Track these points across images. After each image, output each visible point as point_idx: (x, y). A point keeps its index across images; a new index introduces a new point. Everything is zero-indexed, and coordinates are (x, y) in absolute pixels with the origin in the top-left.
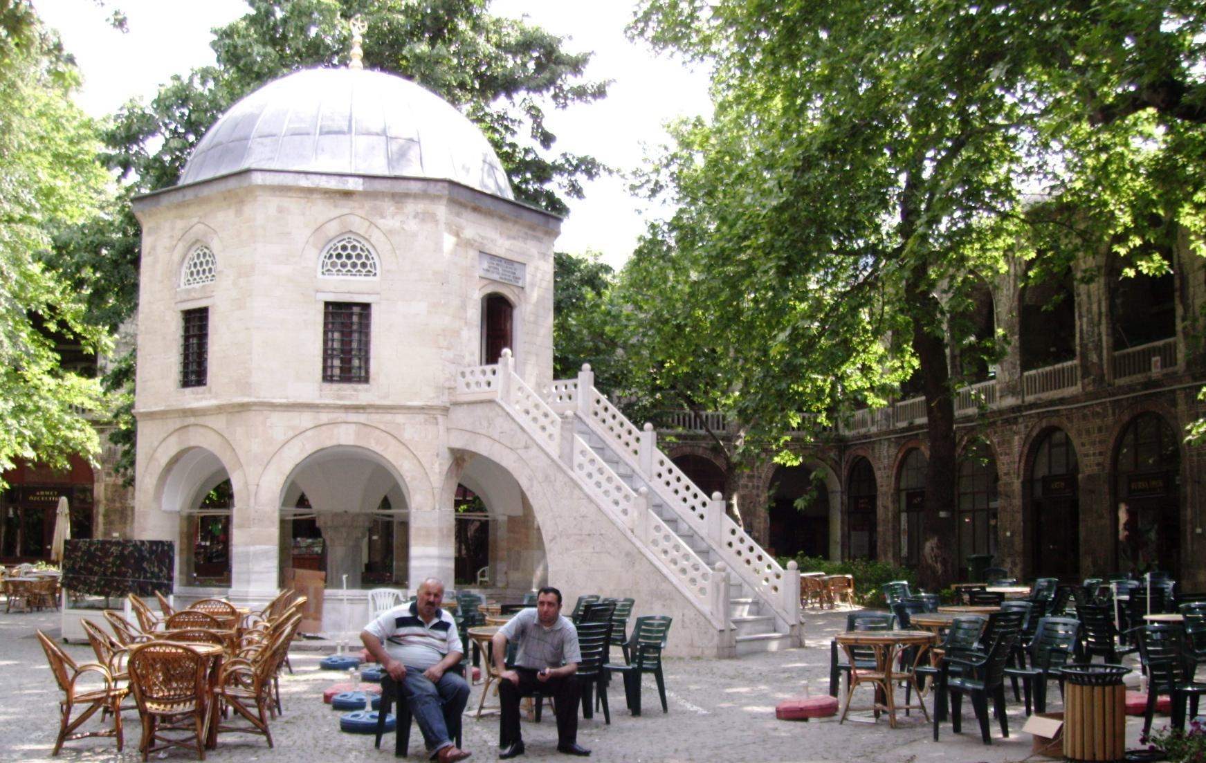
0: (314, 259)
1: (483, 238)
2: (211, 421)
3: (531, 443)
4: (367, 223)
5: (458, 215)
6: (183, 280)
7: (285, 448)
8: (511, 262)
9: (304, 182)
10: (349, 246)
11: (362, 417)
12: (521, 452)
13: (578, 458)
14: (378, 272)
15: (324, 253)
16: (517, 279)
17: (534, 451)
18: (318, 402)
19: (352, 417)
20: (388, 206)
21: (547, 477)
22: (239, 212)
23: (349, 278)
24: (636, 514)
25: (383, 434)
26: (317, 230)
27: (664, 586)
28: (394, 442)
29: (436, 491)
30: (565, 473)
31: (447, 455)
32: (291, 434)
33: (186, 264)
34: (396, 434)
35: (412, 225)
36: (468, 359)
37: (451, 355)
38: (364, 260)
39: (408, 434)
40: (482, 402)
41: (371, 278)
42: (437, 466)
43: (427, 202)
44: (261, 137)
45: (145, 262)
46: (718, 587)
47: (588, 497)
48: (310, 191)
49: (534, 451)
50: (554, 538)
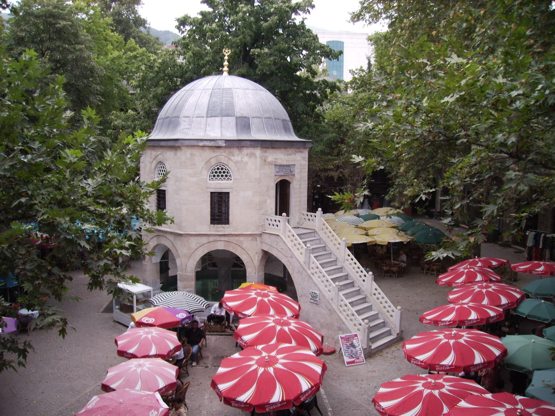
0: (206, 174)
1: (276, 159)
2: (169, 236)
3: (292, 256)
5: (265, 152)
6: (156, 176)
8: (289, 166)
9: (201, 144)
11: (226, 239)
12: (290, 259)
13: (312, 265)
15: (210, 171)
16: (291, 172)
18: (209, 233)
19: (223, 238)
20: (236, 151)
22: (175, 155)
23: (220, 181)
24: (334, 293)
27: (343, 326)
31: (261, 252)
32: (198, 245)
35: (246, 159)
36: (270, 211)
37: (262, 212)
38: (226, 174)
40: (274, 234)
41: (229, 181)
42: (256, 257)
46: (365, 331)
47: (315, 283)
48: (204, 147)
49: (294, 259)
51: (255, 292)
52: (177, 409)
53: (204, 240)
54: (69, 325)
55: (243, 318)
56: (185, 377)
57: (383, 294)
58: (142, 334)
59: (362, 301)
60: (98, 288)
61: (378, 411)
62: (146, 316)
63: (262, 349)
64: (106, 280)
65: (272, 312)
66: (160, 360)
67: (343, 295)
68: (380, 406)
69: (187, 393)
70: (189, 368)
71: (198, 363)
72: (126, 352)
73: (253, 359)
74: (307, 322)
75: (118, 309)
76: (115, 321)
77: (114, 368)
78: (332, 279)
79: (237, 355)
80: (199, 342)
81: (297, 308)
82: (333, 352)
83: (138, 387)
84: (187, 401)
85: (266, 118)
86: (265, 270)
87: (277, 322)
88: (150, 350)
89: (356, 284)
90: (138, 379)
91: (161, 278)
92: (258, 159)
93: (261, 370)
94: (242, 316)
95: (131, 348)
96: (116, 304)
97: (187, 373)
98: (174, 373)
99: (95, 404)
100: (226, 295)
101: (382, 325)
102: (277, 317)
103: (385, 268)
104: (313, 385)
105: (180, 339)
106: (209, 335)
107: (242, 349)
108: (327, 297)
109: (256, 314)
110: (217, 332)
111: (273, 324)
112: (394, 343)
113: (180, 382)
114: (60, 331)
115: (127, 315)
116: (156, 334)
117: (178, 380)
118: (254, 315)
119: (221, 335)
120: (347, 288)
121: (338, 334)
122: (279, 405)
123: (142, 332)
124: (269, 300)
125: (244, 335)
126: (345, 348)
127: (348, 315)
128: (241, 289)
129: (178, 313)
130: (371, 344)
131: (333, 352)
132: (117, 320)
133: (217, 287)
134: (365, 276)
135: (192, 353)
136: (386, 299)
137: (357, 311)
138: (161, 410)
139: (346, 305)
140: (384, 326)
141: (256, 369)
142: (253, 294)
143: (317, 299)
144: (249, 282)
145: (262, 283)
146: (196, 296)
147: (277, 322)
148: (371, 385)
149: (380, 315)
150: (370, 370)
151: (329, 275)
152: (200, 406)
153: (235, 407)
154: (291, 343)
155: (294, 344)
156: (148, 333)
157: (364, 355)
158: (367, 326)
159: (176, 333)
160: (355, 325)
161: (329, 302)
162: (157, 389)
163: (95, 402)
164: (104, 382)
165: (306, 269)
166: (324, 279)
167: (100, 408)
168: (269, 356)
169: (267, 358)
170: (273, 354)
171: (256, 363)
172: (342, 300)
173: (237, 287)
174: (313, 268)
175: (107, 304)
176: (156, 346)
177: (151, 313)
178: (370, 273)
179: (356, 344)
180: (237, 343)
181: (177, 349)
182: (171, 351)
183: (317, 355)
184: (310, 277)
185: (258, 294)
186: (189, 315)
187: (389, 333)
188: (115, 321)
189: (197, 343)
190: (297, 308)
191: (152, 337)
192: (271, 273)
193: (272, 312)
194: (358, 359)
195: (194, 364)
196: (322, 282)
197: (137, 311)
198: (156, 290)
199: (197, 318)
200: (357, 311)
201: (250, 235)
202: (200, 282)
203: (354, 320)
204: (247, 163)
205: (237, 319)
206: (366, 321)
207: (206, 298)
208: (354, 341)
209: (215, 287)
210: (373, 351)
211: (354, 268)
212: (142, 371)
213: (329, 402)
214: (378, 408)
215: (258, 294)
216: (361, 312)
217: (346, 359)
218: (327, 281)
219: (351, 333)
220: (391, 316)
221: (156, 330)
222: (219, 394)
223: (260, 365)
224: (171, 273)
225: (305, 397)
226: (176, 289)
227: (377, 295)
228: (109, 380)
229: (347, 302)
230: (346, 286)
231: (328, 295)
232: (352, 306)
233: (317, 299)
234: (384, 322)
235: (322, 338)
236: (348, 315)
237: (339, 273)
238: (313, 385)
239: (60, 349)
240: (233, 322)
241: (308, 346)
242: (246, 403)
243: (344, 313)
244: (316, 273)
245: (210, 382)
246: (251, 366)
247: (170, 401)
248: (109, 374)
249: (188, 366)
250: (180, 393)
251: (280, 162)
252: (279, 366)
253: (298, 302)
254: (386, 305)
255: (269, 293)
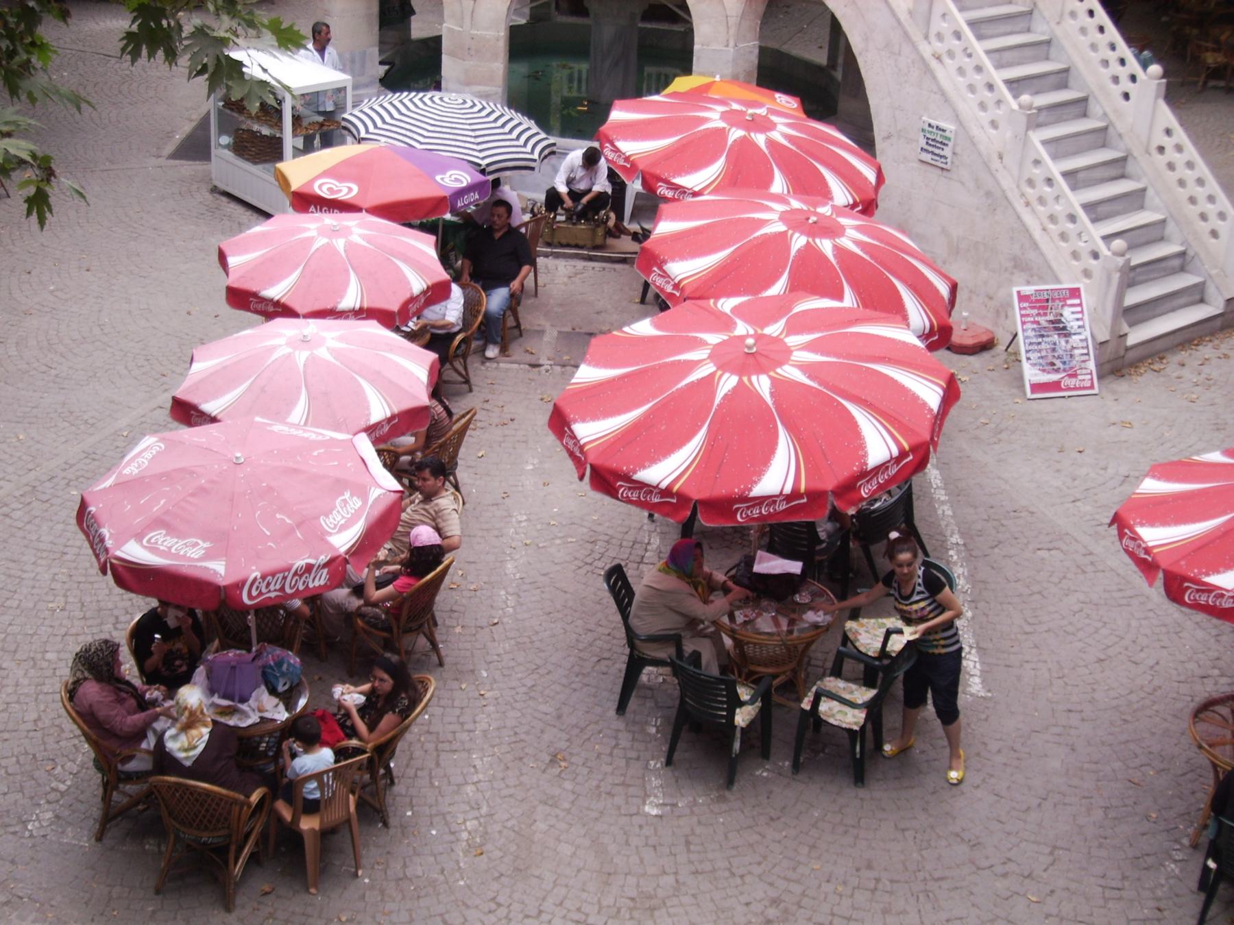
13: (938, 25)
24: (1009, 134)
27: (1031, 255)
29: (732, 21)
30: (915, 47)
45: (375, 454)
47: (943, 93)
51: (721, 109)
52: (428, 497)
54: (64, 182)
55: (673, 200)
56: (459, 394)
57: (1191, 152)
58: (313, 233)
59: (1112, 172)
60: (160, 54)
61: (1131, 554)
62: (326, 174)
63: (735, 310)
64: (187, 29)
65: (779, 184)
66: (373, 328)
67: (1045, 143)
68: (1136, 538)
69: (462, 451)
70: (474, 364)
71: (504, 350)
72: (255, 295)
73: (702, 343)
74: (903, 232)
75: (227, 147)
76: (215, 190)
77: (214, 346)
78: (1009, 83)
79: (644, 327)
80: (514, 278)
81: (871, 176)
82: (986, 346)
83: (299, 412)
84: (462, 474)
86: (761, 37)
87: (796, 221)
88: (342, 292)
89: (1094, 108)
90: (299, 388)
91: (382, 43)
93: (728, 383)
94: (669, 194)
95: (272, 282)
96: (222, 131)
97: (467, 381)
98: (422, 375)
99: (151, 461)
100: (618, 115)
101: (1176, 263)
102: (796, 204)
103: (1211, 59)
104: (906, 447)
105: (444, 259)
106: (546, 255)
107: (664, 307)
108: (982, 148)
109: (720, 186)
110: (577, 246)
111: (781, 227)
112: (1213, 333)
113: (440, 409)
114: (29, 201)
115: (257, 170)
116: (363, 237)
117: (435, 403)
118: (715, 191)
119: (590, 259)
120: (1058, 121)
121: (1011, 283)
122: (783, 506)
123: (314, 225)
124: (771, 143)
125: (673, 260)
126: (1030, 333)
127: (1053, 219)
128: (675, 95)
129: (443, 169)
130: (1125, 328)
131: (986, 346)
132: (222, 187)
133: (584, 95)
134: (1133, 78)
135: (487, 316)
136: (1203, 169)
137: (1089, 207)
138: (375, 493)
139: (1049, 181)
140: (1182, 269)
141: (712, 375)
142: (714, 118)
143: (947, 152)
144: (702, 74)
145: (749, 82)
146: (509, 113)
147: (796, 221)
148: (1111, 471)
149: (1171, 228)
150: (1114, 418)
151: (999, 66)
152: (506, 495)
153: (628, 501)
154: (839, 296)
155: (849, 300)
156: (334, 232)
157: (1099, 365)
158: (1120, 261)
159: (433, 238)
160: (1075, 255)
161: (986, 165)
162: (363, 425)
163: (148, 455)
164: (180, 393)
165: (917, 36)
166: (977, 78)
167: (167, 477)
168: (759, 338)
169: (750, 341)
170: (774, 330)
171: (711, 357)
172: (1037, 162)
173: (658, 92)
174: (940, 37)
175: (188, 128)
176: (361, 278)
177: (347, 163)
178: (1156, 69)
179: (1073, 325)
180: (646, 286)
181: (438, 293)
182: (412, 299)
183: (932, 347)
184: (928, 70)
185: (732, 118)
186: (481, 178)
187: (1197, 295)
188: (215, 190)
189: (505, 280)
190: (871, 176)
191: (350, 247)
192: (785, 48)
193: (779, 184)
194: (1074, 375)
195: (492, 352)
196: (972, 88)
197: (294, 157)
198: (366, 86)
199: (509, 192)
200: (1089, 207)
202: (523, 68)
203: (1073, 236)
205: (650, 206)
206: (1118, 244)
207: (544, 125)
208: (1067, 313)
209: (575, 94)
210: (1131, 355)
211: (1094, 47)
212: (313, 361)
213: (954, 517)
214: (1131, 545)
215: (732, 118)
216: (1102, 209)
217: (1032, 374)
218: (990, 87)
219: (1058, 281)
220: (1214, 234)
221: (360, 226)
222: (577, 455)
223: (724, 367)
224: (419, 29)
225: (873, 486)
226: (438, 87)
227: (1171, 155)
228: (196, 386)
229: (1055, 169)
230: (1057, 111)
231: (989, 140)
232: (1074, 188)
233: (947, 152)
234: (1182, 254)
235: (954, 288)
236: (1053, 219)
237: (1036, 59)
238: (906, 447)
239: (25, 277)
240: (634, 216)
241: (896, 311)
242: (667, 492)
243: (1040, 208)
244: (951, 54)
245: (543, 418)
246: (692, 365)
247: (405, 471)
248: (196, 367)
249: (469, 360)
250: (441, 446)
252: (790, 372)
253: (874, 155)
254: (1200, 192)
255: (774, 118)
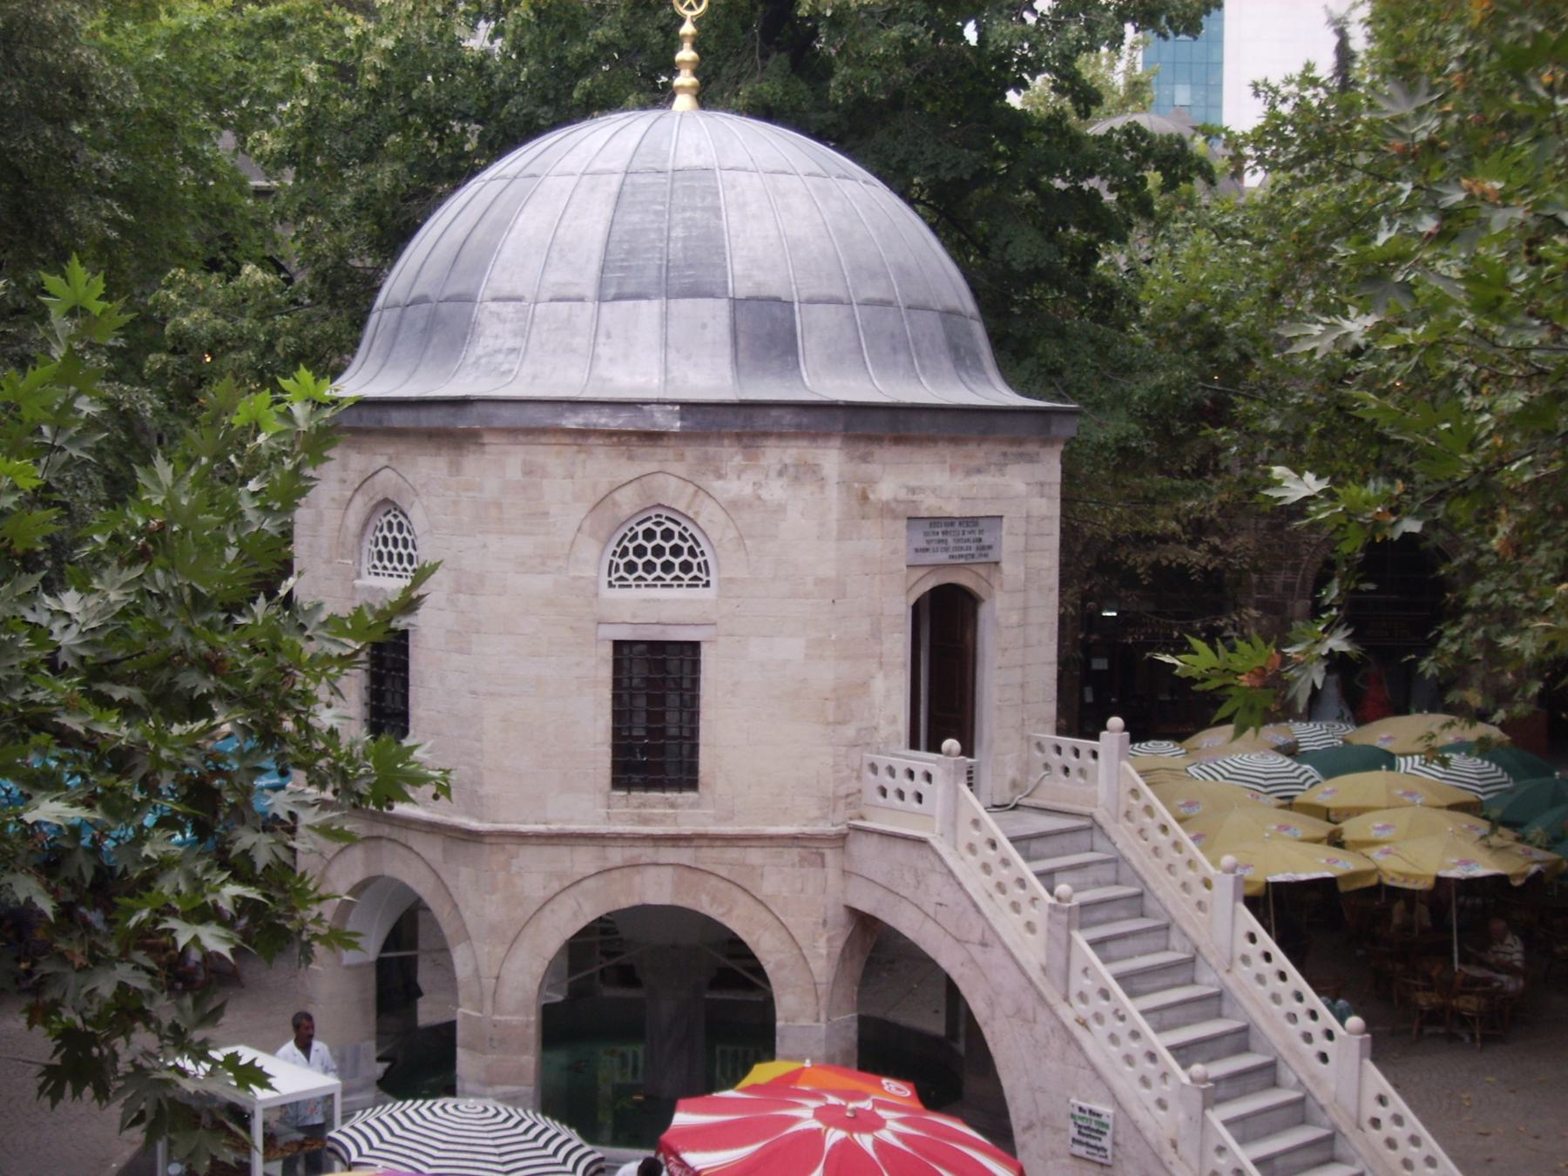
0: (593, 560)
1: (913, 490)
2: (418, 841)
4: (691, 489)
5: (865, 459)
6: (366, 565)
7: (547, 910)
8: (972, 521)
9: (573, 421)
10: (658, 530)
11: (684, 855)
12: (976, 950)
13: (1079, 983)
14: (713, 578)
15: (612, 547)
17: (996, 955)
18: (603, 828)
19: (668, 854)
20: (731, 455)
21: (1019, 1011)
22: (456, 468)
25: (723, 885)
26: (594, 507)
28: (742, 898)
29: (821, 989)
30: (1054, 1013)
31: (843, 917)
32: (555, 886)
33: (370, 537)
34: (748, 886)
35: (776, 490)
36: (884, 730)
37: (850, 731)
38: (685, 557)
39: (770, 886)
40: (905, 838)
41: (699, 593)
43: (804, 443)
44: (495, 300)
48: (583, 433)
49: (996, 955)
50: (1030, 1127)
53: (583, 860)
85: (868, 303)
92: (833, 493)
201: (794, 839)
204: (781, 508)
251: (930, 505)
